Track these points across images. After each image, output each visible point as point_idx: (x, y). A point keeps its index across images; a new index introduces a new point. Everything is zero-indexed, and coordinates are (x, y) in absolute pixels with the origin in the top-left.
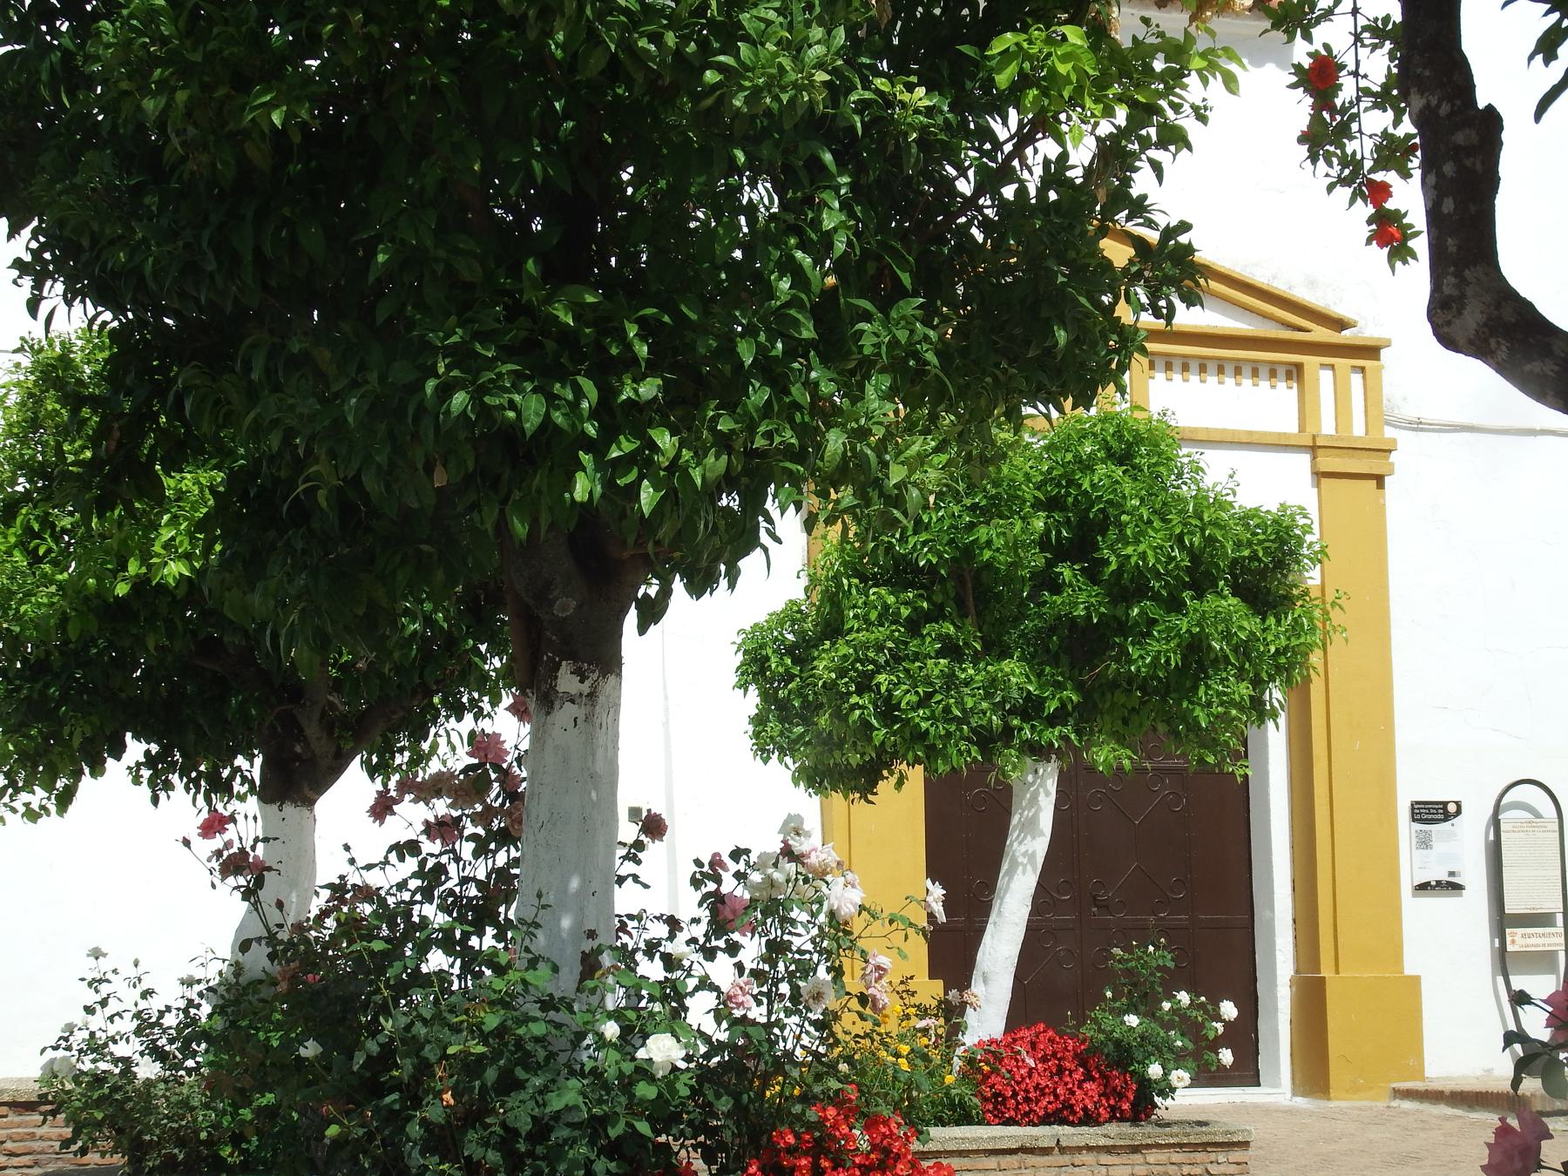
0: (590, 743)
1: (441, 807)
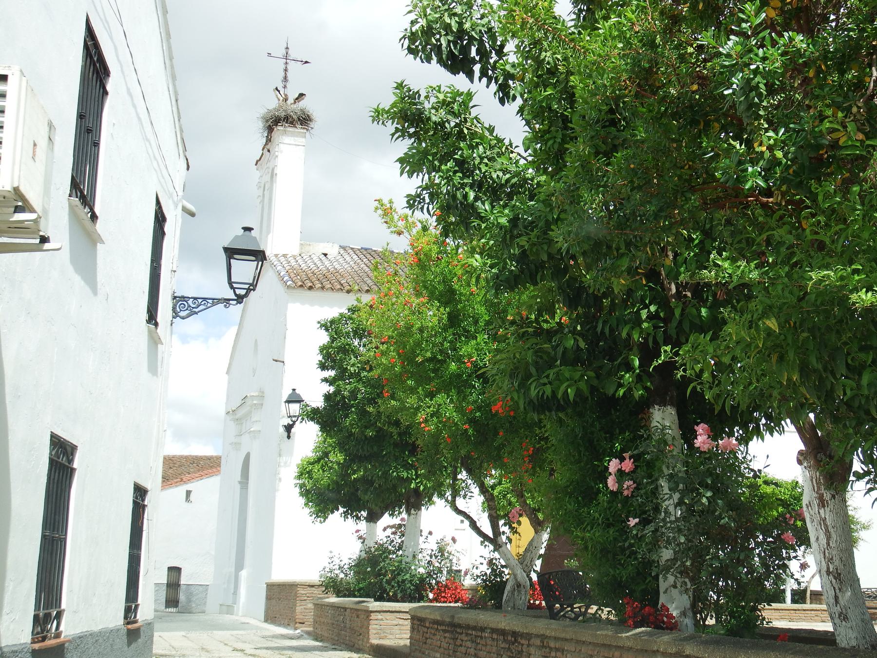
0: (416, 522)
1: (394, 530)
